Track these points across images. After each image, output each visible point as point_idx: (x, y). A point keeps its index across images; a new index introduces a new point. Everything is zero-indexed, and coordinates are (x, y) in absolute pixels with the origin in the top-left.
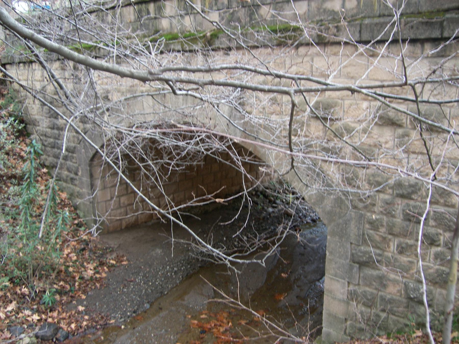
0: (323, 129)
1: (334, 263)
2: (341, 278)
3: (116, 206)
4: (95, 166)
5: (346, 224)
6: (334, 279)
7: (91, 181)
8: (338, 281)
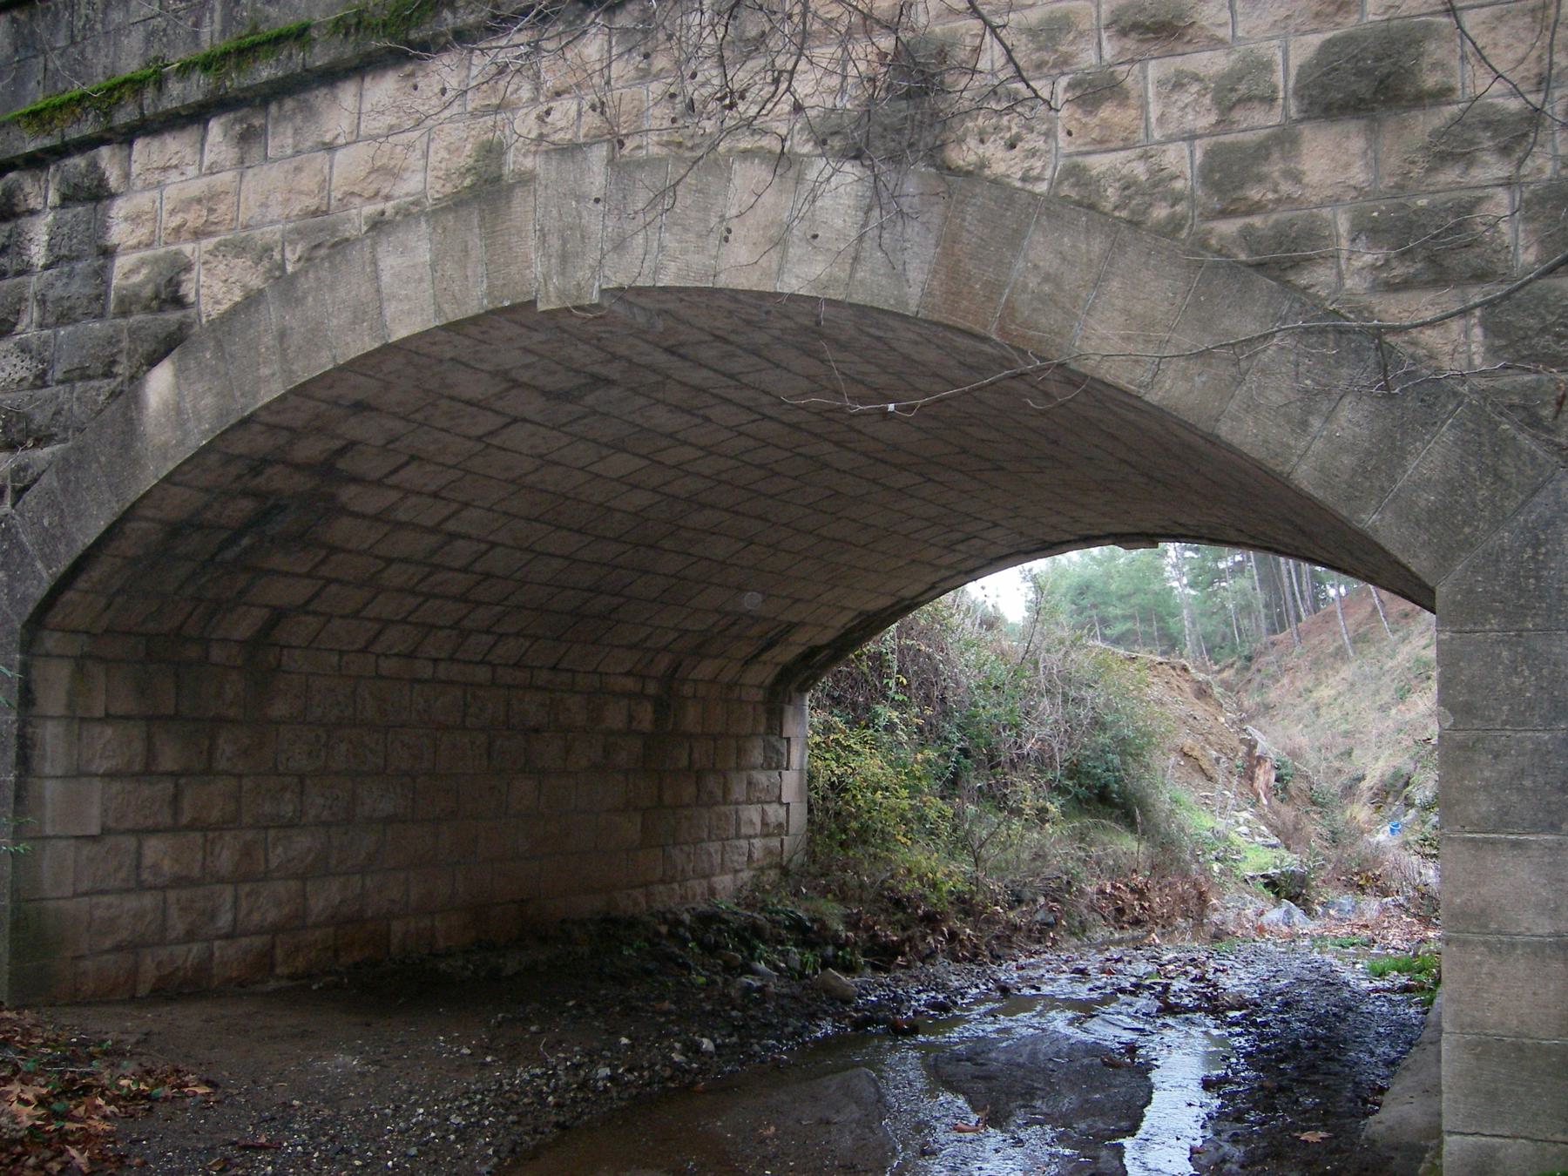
0: (1365, 153)
1: (1485, 758)
2: (1536, 827)
3: (122, 875)
4: (48, 655)
5: (1536, 544)
6: (1493, 843)
7: (24, 723)
8: (1515, 845)
